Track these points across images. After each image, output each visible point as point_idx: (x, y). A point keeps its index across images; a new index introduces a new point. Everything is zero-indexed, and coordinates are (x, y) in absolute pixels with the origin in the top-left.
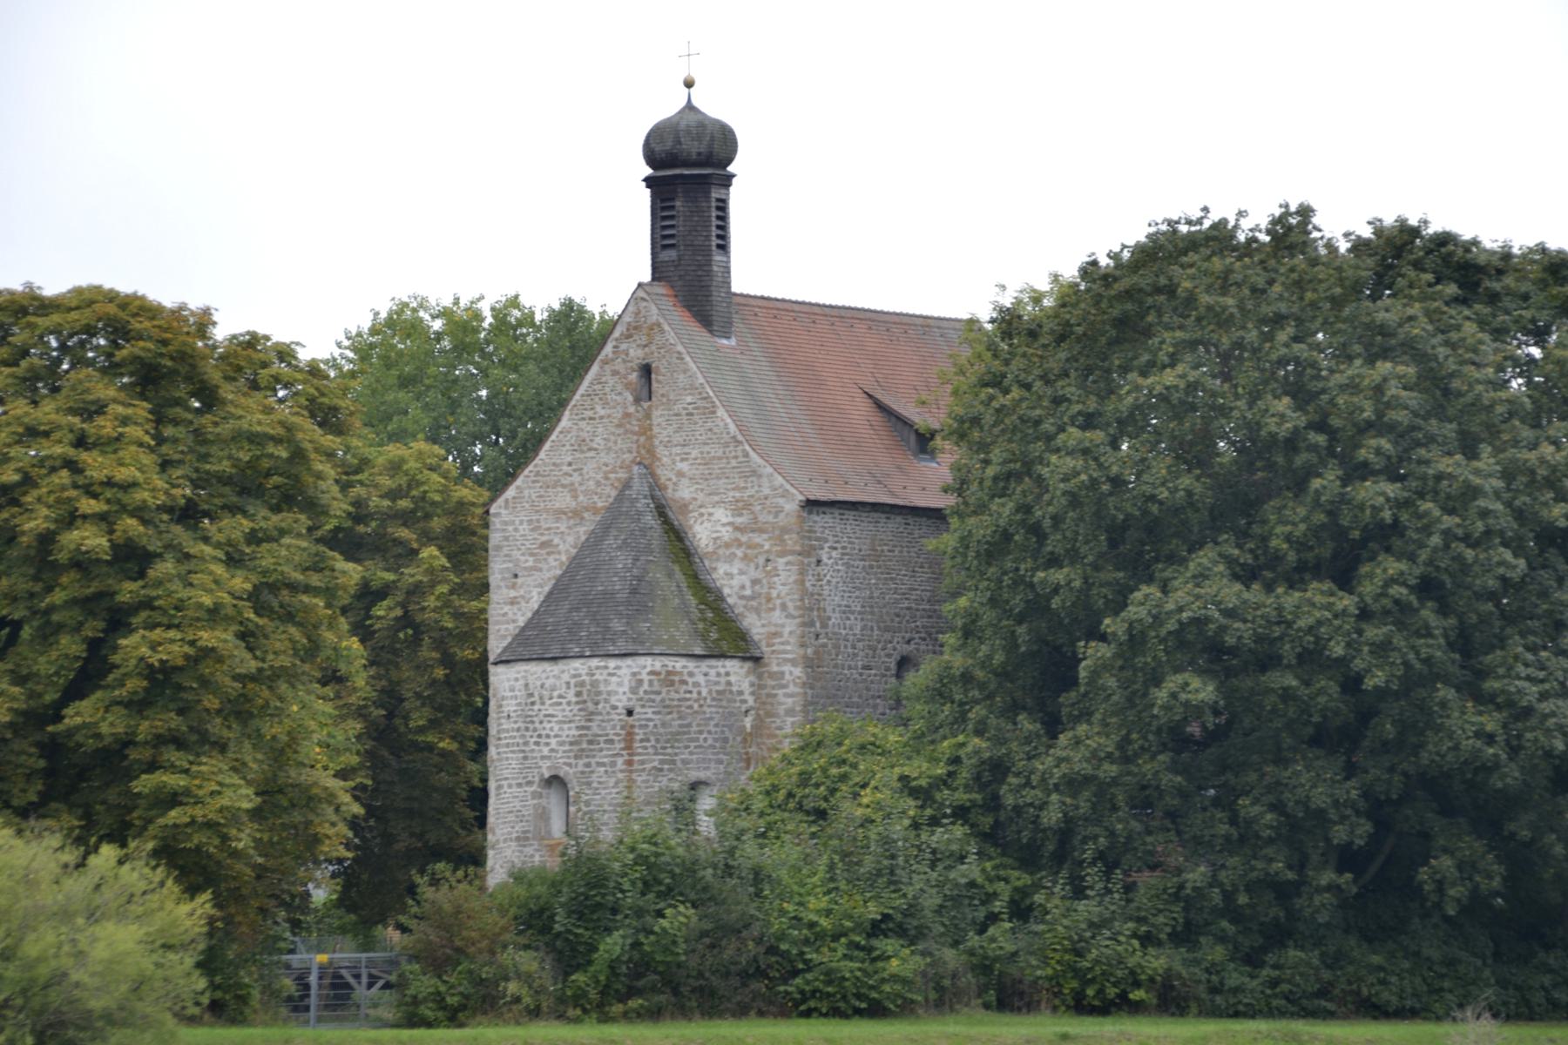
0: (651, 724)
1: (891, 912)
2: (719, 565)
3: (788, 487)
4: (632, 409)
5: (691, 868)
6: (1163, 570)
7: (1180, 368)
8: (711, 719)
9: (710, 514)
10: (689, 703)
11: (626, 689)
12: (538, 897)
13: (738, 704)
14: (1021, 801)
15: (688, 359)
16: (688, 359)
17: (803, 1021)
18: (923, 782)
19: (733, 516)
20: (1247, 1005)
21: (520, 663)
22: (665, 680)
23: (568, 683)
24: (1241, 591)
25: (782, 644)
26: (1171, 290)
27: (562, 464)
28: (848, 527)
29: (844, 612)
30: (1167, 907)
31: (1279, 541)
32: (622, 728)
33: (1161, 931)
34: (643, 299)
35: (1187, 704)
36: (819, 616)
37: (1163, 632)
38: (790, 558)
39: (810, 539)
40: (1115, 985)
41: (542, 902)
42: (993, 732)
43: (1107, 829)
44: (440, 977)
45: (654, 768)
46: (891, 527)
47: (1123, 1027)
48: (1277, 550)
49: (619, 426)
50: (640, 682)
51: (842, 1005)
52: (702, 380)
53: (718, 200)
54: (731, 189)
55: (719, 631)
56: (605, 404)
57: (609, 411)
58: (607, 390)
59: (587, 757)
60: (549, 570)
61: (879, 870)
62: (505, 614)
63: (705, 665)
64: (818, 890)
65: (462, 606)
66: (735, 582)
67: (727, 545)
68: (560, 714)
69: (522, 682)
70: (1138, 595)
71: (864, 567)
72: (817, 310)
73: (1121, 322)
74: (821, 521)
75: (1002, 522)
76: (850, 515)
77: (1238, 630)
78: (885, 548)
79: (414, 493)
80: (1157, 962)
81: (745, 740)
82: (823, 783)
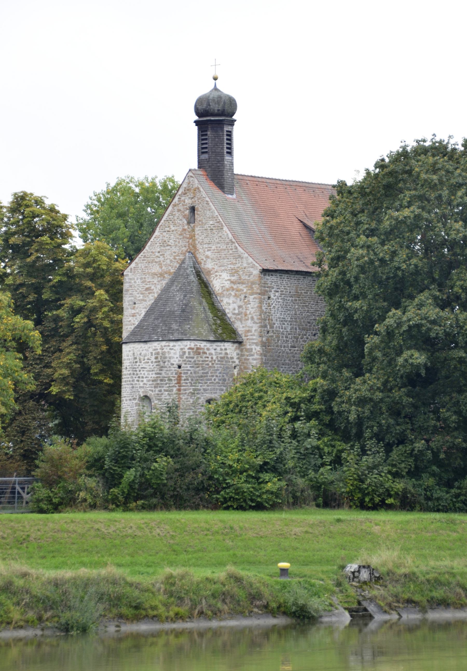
0: (189, 372)
1: (269, 461)
2: (224, 299)
3: (255, 263)
4: (186, 227)
5: (172, 440)
6: (405, 302)
7: (412, 208)
8: (217, 370)
9: (220, 276)
10: (207, 363)
11: (178, 356)
12: (98, 453)
13: (231, 363)
14: (341, 409)
15: (211, 204)
16: (211, 204)
17: (226, 512)
18: (297, 400)
19: (230, 276)
20: (443, 506)
21: (131, 344)
22: (196, 352)
23: (152, 353)
24: (439, 312)
25: (252, 335)
26: (409, 172)
27: (155, 252)
28: (284, 282)
29: (282, 321)
30: (407, 459)
31: (458, 289)
32: (176, 374)
33: (402, 471)
34: (191, 177)
35: (412, 364)
36: (269, 323)
37: (401, 331)
38: (255, 296)
39: (265, 287)
40: (379, 496)
41: (100, 454)
42: (330, 377)
43: (378, 423)
44: (50, 489)
45: (191, 392)
46: (305, 282)
47: (368, 516)
48: (457, 293)
49: (181, 235)
50: (184, 353)
51: (244, 504)
52: (217, 214)
53: (227, 131)
54: (234, 127)
55: (222, 329)
56: (175, 225)
57: (176, 228)
58: (176, 218)
59: (160, 387)
60: (149, 301)
61: (264, 441)
62: (130, 321)
63: (215, 345)
64: (235, 450)
65: (114, 317)
66: (231, 307)
67: (228, 290)
68: (148, 367)
69: (132, 352)
70: (391, 314)
71: (292, 300)
72: (278, 182)
73: (388, 187)
74: (270, 279)
75: (334, 280)
76: (285, 276)
77: (436, 330)
78: (303, 291)
79: (94, 265)
80: (399, 485)
81: (234, 380)
82: (251, 400)
